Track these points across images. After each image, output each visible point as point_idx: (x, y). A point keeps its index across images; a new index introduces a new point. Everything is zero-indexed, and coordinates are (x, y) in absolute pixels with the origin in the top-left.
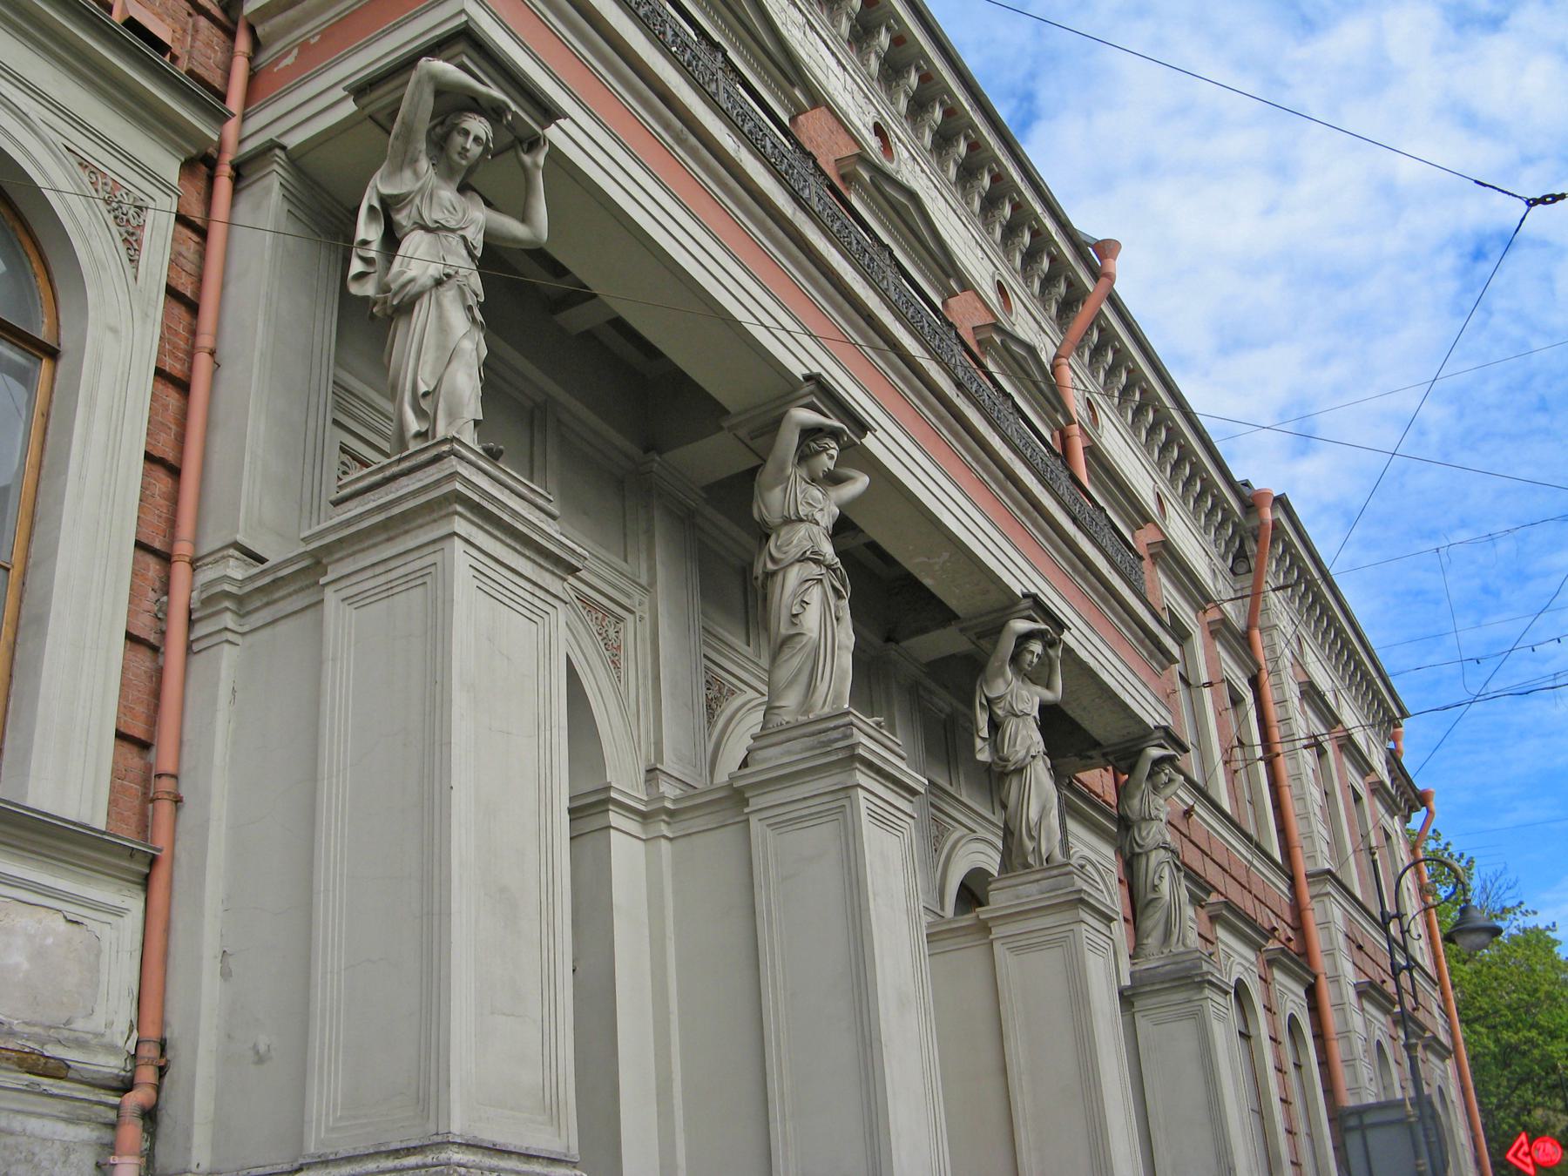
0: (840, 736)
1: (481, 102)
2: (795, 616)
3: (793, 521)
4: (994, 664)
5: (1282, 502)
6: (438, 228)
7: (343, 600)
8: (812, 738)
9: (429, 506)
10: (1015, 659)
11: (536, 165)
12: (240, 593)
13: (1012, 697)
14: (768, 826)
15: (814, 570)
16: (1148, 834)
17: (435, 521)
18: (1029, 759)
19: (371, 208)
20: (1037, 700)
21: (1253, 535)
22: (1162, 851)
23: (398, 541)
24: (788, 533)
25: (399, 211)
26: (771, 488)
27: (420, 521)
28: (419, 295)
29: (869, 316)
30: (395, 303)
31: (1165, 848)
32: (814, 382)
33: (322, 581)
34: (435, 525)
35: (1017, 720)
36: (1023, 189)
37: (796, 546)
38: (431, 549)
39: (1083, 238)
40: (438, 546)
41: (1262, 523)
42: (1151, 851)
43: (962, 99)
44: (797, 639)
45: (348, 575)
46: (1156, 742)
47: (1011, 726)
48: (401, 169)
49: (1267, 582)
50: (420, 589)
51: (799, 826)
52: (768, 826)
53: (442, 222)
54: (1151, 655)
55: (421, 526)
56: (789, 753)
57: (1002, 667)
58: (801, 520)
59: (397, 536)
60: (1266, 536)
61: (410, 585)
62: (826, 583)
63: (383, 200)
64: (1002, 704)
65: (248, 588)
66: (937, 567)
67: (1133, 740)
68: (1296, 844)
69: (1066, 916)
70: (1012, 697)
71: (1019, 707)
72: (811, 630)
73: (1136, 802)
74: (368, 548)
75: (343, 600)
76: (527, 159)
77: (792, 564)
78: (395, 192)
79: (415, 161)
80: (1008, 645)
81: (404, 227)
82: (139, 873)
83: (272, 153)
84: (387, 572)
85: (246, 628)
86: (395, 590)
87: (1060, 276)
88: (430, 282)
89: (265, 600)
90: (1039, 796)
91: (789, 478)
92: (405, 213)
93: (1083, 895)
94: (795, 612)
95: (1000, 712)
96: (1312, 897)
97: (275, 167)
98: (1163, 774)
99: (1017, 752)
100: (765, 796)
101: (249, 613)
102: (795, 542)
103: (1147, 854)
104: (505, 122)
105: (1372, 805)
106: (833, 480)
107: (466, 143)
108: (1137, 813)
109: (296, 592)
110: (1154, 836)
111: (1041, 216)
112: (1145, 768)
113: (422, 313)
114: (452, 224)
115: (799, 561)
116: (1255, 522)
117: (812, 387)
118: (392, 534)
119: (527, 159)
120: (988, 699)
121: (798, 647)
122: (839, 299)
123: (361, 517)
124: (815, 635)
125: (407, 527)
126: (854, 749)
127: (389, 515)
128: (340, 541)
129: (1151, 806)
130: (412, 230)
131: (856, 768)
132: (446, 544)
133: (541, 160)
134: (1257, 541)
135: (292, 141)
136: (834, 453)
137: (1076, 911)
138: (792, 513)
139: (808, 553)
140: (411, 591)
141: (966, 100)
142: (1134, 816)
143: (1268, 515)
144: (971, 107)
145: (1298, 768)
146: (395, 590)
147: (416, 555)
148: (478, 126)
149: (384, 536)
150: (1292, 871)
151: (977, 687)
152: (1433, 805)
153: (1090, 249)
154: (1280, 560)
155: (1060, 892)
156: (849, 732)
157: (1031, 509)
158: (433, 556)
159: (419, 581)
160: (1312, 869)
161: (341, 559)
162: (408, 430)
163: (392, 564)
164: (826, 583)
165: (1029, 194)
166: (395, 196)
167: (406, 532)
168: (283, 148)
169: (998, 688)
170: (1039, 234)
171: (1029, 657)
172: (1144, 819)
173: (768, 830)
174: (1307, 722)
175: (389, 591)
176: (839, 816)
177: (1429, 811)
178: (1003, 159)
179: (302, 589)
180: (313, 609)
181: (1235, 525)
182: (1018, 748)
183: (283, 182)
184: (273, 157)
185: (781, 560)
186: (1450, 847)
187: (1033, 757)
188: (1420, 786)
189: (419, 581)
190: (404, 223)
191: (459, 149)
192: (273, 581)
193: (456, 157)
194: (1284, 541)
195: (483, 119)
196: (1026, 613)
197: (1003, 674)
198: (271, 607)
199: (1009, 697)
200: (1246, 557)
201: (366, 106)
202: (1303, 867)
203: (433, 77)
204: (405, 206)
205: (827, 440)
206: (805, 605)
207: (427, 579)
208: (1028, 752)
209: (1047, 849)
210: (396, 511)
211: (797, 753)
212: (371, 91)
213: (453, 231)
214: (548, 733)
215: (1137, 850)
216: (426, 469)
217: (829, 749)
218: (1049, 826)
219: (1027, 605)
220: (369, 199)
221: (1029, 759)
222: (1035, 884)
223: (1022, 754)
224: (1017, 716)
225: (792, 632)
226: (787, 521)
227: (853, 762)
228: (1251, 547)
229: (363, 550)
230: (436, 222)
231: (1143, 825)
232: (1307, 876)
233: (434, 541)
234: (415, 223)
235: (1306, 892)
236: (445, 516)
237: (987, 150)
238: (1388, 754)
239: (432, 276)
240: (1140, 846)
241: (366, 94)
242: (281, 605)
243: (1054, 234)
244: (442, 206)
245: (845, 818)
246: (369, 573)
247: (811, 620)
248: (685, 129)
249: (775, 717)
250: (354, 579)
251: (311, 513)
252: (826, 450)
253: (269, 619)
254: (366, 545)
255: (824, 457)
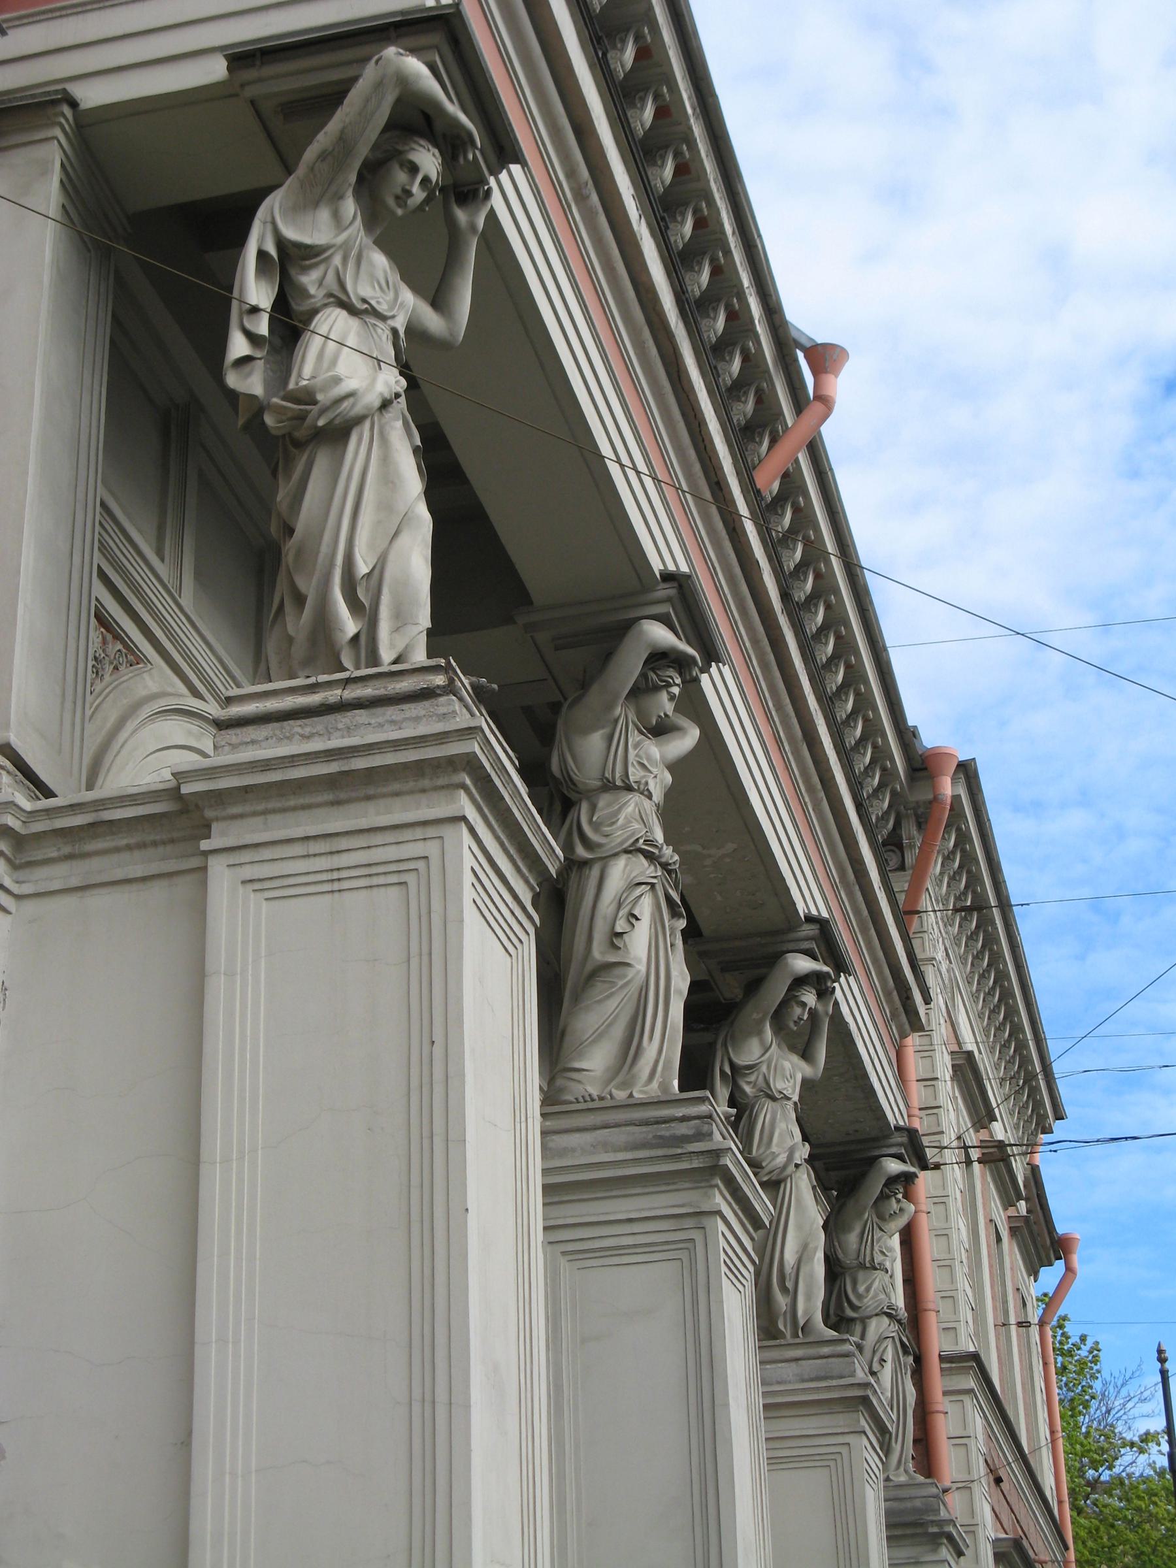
0: (691, 1132)
1: (438, 126)
2: (620, 935)
3: (617, 788)
4: (751, 1013)
5: (967, 771)
6: (365, 311)
7: (244, 882)
8: (644, 1129)
9: (419, 768)
10: (779, 1018)
11: (473, 227)
12: (23, 832)
13: (769, 1067)
14: (564, 1253)
15: (643, 869)
16: (868, 1290)
17: (423, 791)
18: (791, 1168)
19: (262, 255)
20: (799, 1077)
21: (917, 817)
22: (886, 1320)
23: (353, 808)
24: (609, 805)
25: (305, 269)
26: (587, 730)
27: (396, 786)
28: (359, 420)
29: (718, 483)
30: (321, 423)
31: (889, 1315)
32: (675, 584)
33: (205, 845)
34: (423, 798)
35: (774, 1104)
36: (732, 245)
37: (623, 827)
38: (419, 833)
39: (794, 334)
40: (431, 832)
41: (936, 800)
42: (870, 1317)
43: (685, 96)
44: (618, 971)
45: (257, 846)
46: (893, 1150)
47: (766, 1112)
48: (316, 204)
49: (927, 889)
50: (394, 892)
51: (616, 1260)
52: (564, 1253)
53: (373, 302)
54: (894, 1015)
55: (397, 794)
56: (606, 1146)
57: (761, 1022)
58: (629, 788)
59: (349, 801)
60: (940, 820)
61: (375, 881)
62: (659, 888)
63: (282, 244)
64: (752, 1078)
65: (38, 827)
66: (708, 862)
67: (860, 1141)
68: (930, 1306)
69: (839, 1421)
70: (769, 1067)
71: (779, 1085)
72: (639, 961)
73: (852, 1238)
74: (294, 809)
75: (244, 882)
76: (461, 215)
77: (616, 855)
78: (307, 240)
79: (341, 197)
80: (776, 989)
81: (311, 296)
82: (945, 1417)
83: (58, 109)
84: (331, 853)
85: (26, 889)
86: (346, 885)
87: (750, 385)
88: (377, 403)
89: (67, 850)
90: (799, 1227)
91: (616, 721)
92: (315, 275)
93: (869, 1393)
94: (619, 929)
95: (748, 1089)
96: (945, 1393)
97: (57, 132)
98: (893, 1199)
99: (775, 1156)
100: (562, 1206)
101: (30, 864)
102: (620, 822)
103: (864, 1321)
104: (461, 161)
105: (1011, 1250)
106: (660, 730)
107: (412, 184)
108: (853, 1255)
109: (129, 848)
110: (876, 1295)
111: (747, 291)
112: (875, 1186)
113: (357, 447)
114: (383, 308)
115: (626, 851)
116: (922, 795)
117: (672, 592)
118: (342, 795)
119: (461, 215)
120: (732, 1065)
121: (621, 983)
122: (692, 454)
123: (292, 760)
124: (642, 968)
125: (371, 791)
126: (718, 1157)
127: (346, 768)
128: (246, 789)
129: (876, 1248)
130: (326, 305)
131: (717, 1186)
132: (447, 831)
133: (481, 222)
134: (920, 826)
135: (92, 95)
136: (676, 690)
137: (855, 1415)
138: (618, 775)
139: (641, 841)
140: (375, 890)
141: (689, 98)
142: (848, 1260)
143: (948, 787)
144: (694, 109)
145: (944, 1187)
146: (324, 877)
147: (389, 837)
148: (429, 161)
149: (328, 797)
150: (919, 1348)
151: (719, 1046)
152: (1076, 1259)
153: (800, 355)
154: (948, 858)
155: (834, 1383)
156: (706, 1128)
157: (819, 786)
158: (421, 844)
159: (394, 879)
160: (949, 1348)
161: (241, 816)
162: (342, 631)
163: (344, 843)
164: (659, 888)
165: (738, 256)
166: (307, 247)
167: (368, 798)
168: (73, 104)
169: (750, 1052)
170: (738, 318)
171: (798, 1011)
172: (862, 1266)
173: (563, 1261)
174: (958, 1115)
175: (334, 884)
176: (684, 1255)
177: (1069, 1269)
178: (717, 196)
179: (142, 846)
180: (164, 883)
181: (894, 794)
182: (774, 1149)
183: (64, 160)
184: (56, 115)
185: (600, 845)
186: (1066, 1323)
187: (797, 1166)
188: (1061, 1229)
189: (394, 879)
190: (312, 290)
191: (399, 191)
192: (92, 825)
193: (391, 202)
194: (959, 830)
195: (436, 152)
196: (806, 945)
197: (760, 1033)
198: (75, 863)
199: (764, 1068)
200: (900, 847)
201: (249, 83)
202: (937, 1343)
203: (403, 81)
204: (316, 265)
205: (671, 672)
206: (633, 921)
207: (410, 878)
208: (790, 1157)
209: (806, 1312)
210: (360, 763)
211: (617, 1150)
212: (263, 63)
213: (383, 318)
214: (523, 1125)
215: (850, 1313)
216: (405, 707)
217: (679, 1151)
218: (811, 1276)
219: (811, 933)
220: (258, 239)
221: (791, 1168)
222: (793, 1365)
223: (781, 1159)
224: (774, 1099)
225: (612, 958)
226: (608, 786)
227: (713, 1175)
228: (910, 831)
229: (284, 810)
230: (364, 301)
231: (861, 1275)
232: (942, 1359)
233: (425, 823)
234: (330, 295)
235: (938, 1382)
236: (443, 787)
237: (699, 180)
238: (1029, 1172)
239: (381, 394)
240: (854, 1308)
241: (253, 66)
242: (95, 863)
243: (757, 322)
244: (373, 278)
245: (693, 1261)
246: (298, 849)
247: (639, 942)
248: (590, 183)
249: (572, 1084)
250: (267, 854)
251: (75, 703)
252: (669, 685)
253: (74, 882)
254: (292, 803)
255: (664, 696)
